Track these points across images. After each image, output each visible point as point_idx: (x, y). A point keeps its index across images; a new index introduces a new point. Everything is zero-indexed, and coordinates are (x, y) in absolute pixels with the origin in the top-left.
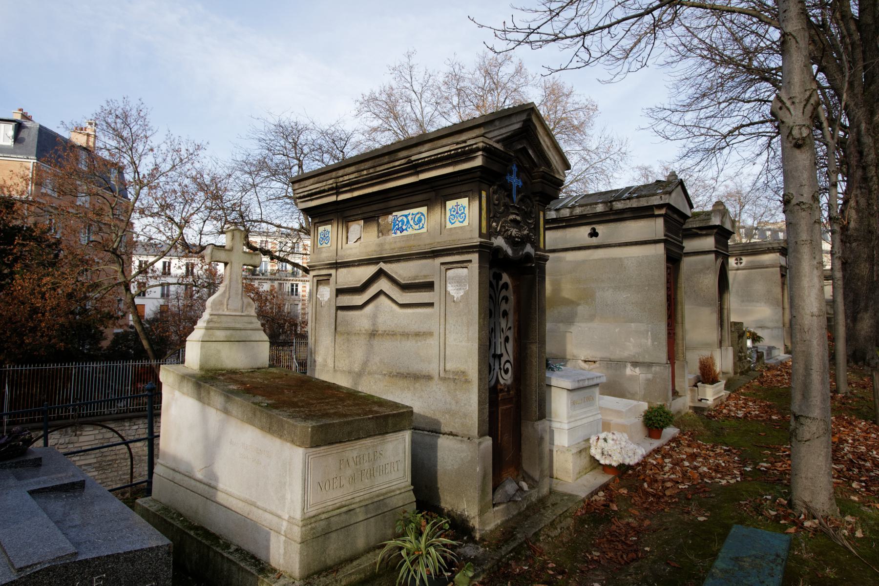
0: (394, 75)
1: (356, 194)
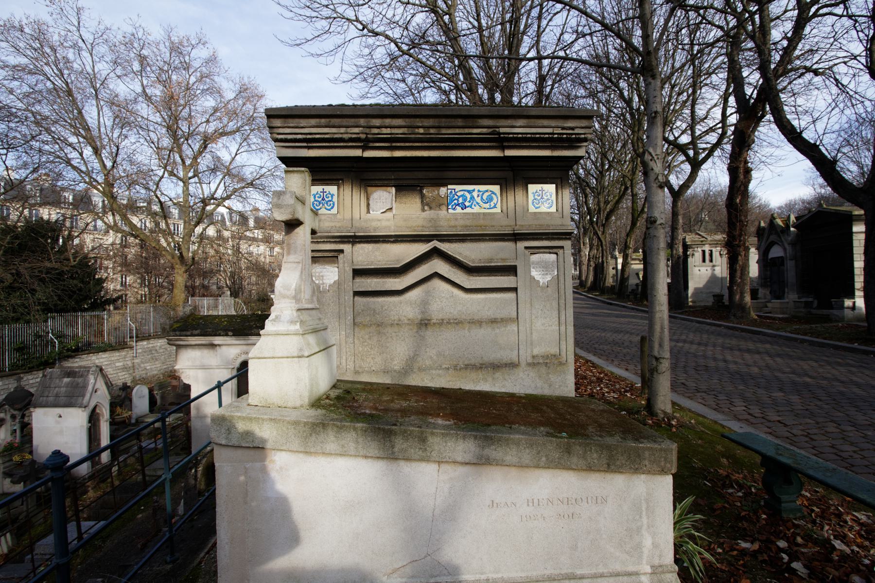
0: (50, 9)
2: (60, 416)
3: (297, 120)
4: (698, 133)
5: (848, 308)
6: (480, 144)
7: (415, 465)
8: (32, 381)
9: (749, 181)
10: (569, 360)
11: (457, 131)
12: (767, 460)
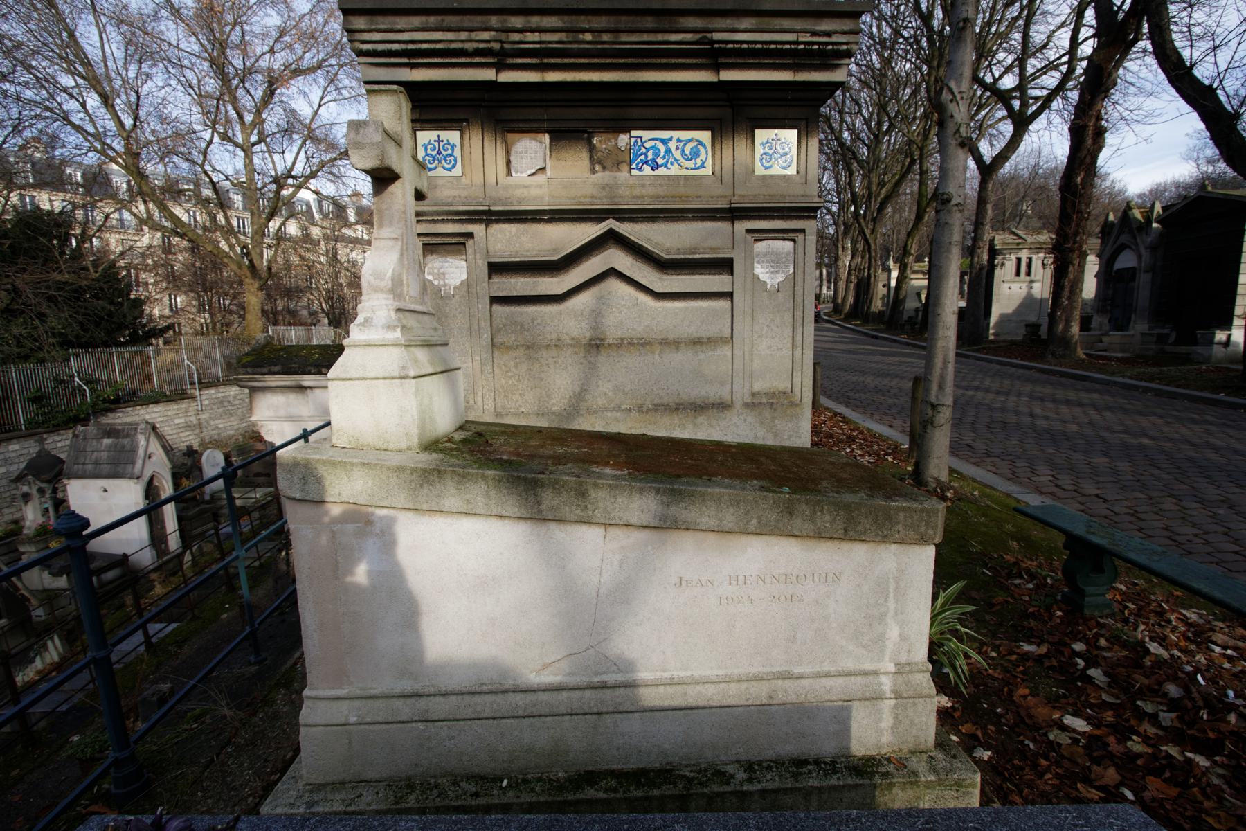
1: (553, 77)
2: (105, 491)
3: (390, 19)
4: (1030, 70)
5: (1219, 343)
6: (681, 61)
7: (570, 528)
8: (59, 443)
9: (1099, 150)
10: (805, 400)
11: (645, 37)
12: (1073, 541)
